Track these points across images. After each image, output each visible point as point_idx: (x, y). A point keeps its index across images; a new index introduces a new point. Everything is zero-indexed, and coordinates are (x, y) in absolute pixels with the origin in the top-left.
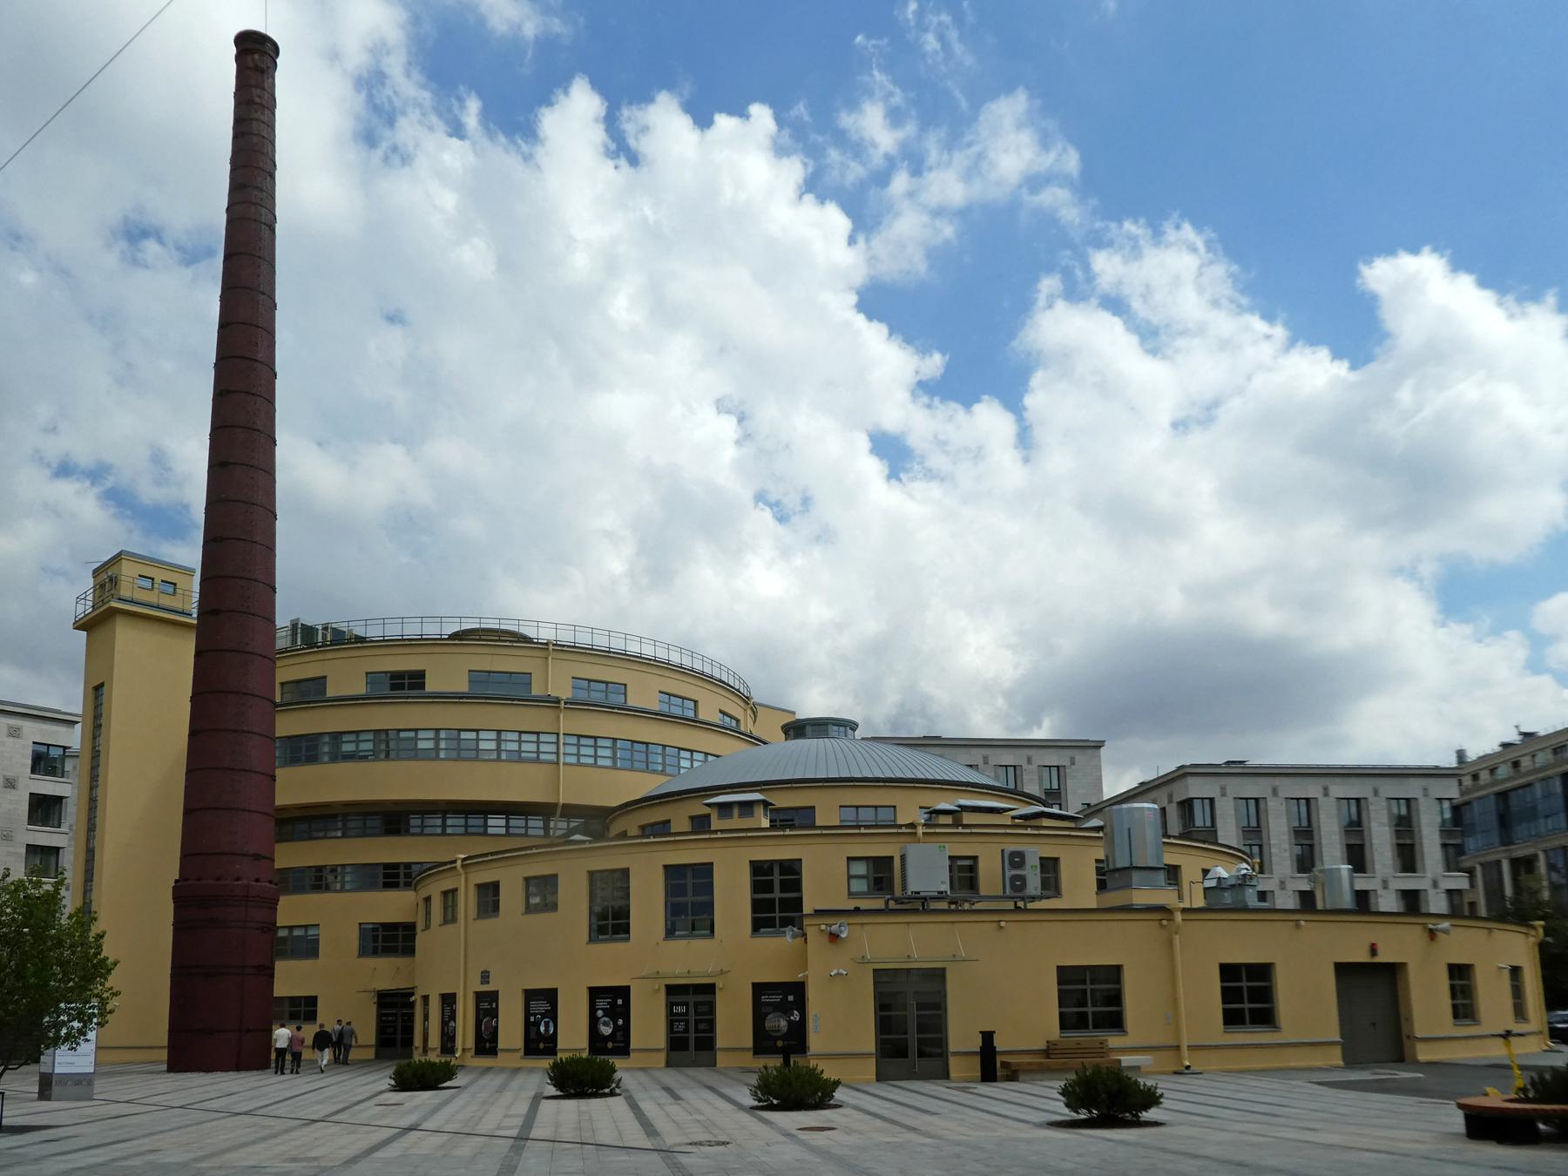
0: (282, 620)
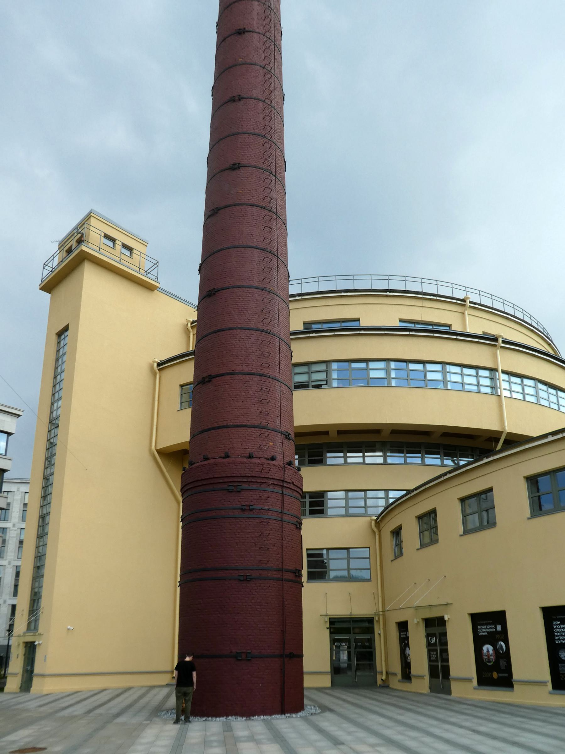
0: (191, 409)
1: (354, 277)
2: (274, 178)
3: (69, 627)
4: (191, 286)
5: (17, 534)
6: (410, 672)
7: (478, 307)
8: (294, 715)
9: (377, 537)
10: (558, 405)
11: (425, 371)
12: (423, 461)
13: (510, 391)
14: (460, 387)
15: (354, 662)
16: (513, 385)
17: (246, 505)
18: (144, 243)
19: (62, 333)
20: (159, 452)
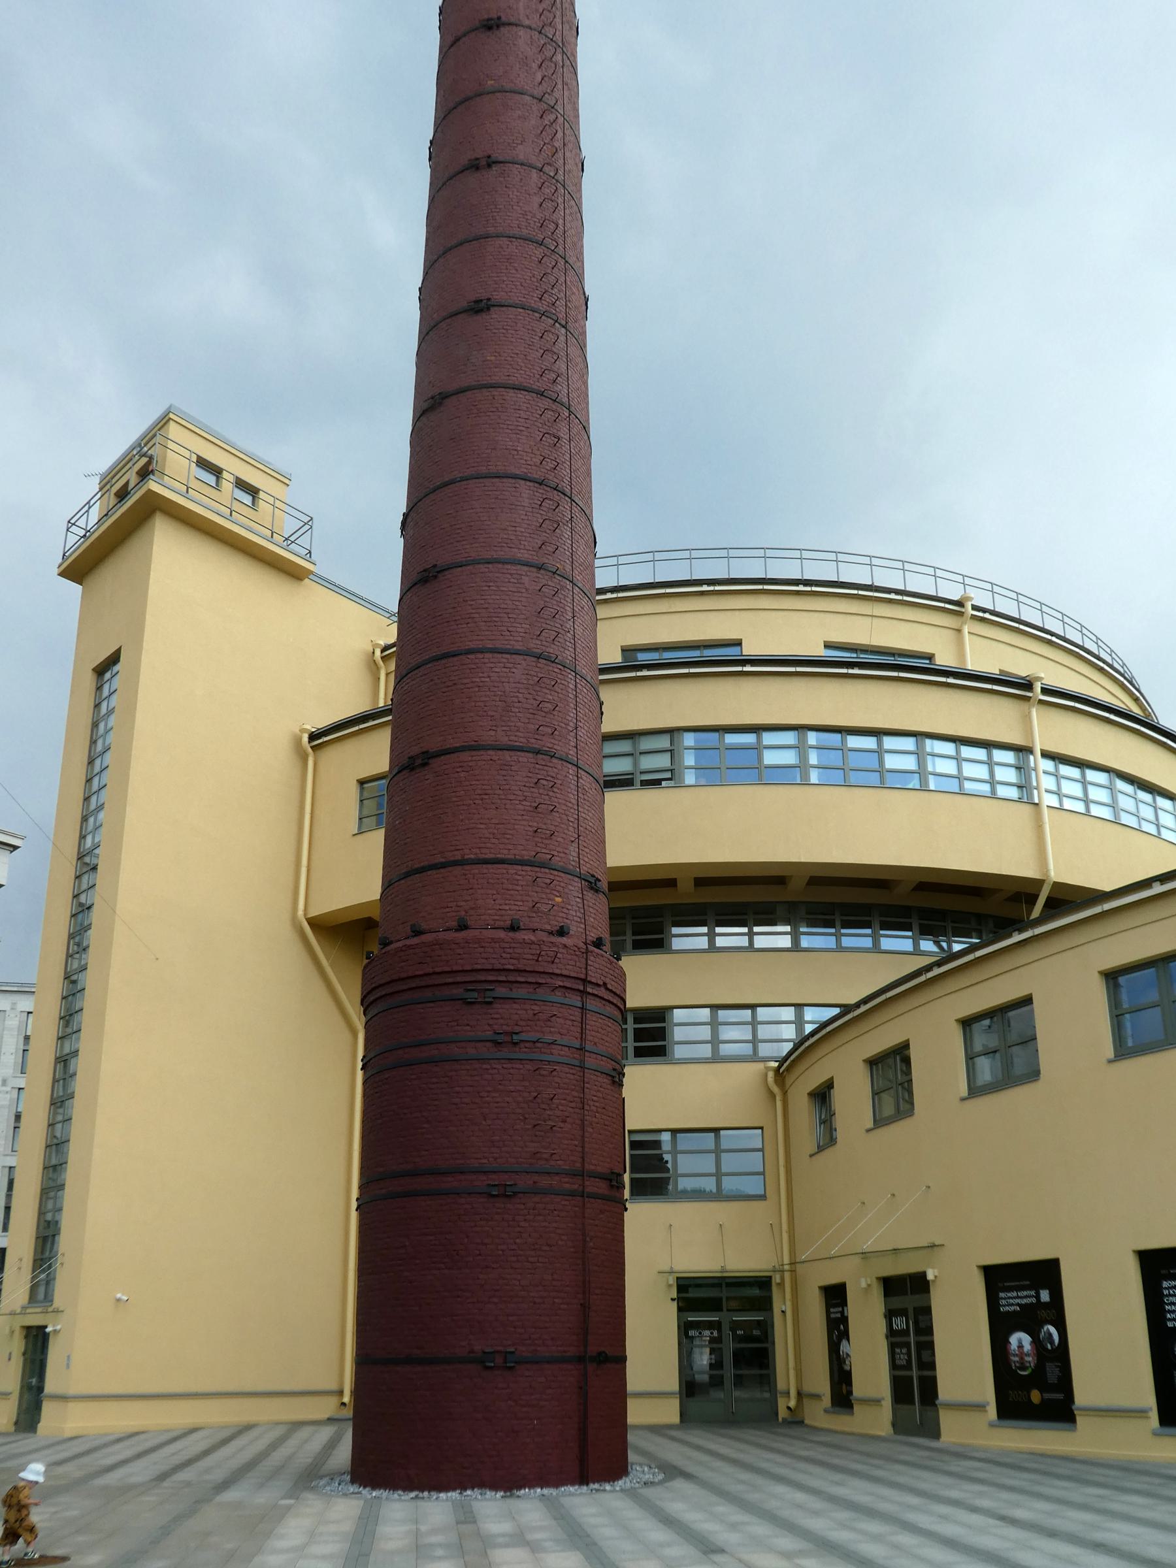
0: (383, 830)
1: (728, 552)
2: (563, 331)
3: (119, 1295)
4: (383, 571)
5: (11, 1099)
6: (851, 1393)
7: (988, 617)
8: (608, 1487)
9: (779, 1104)
10: (1158, 826)
11: (880, 752)
12: (876, 944)
13: (1058, 793)
14: (953, 785)
15: (729, 1371)
16: (1063, 782)
17: (506, 1033)
18: (284, 479)
19: (107, 666)
20: (313, 922)
